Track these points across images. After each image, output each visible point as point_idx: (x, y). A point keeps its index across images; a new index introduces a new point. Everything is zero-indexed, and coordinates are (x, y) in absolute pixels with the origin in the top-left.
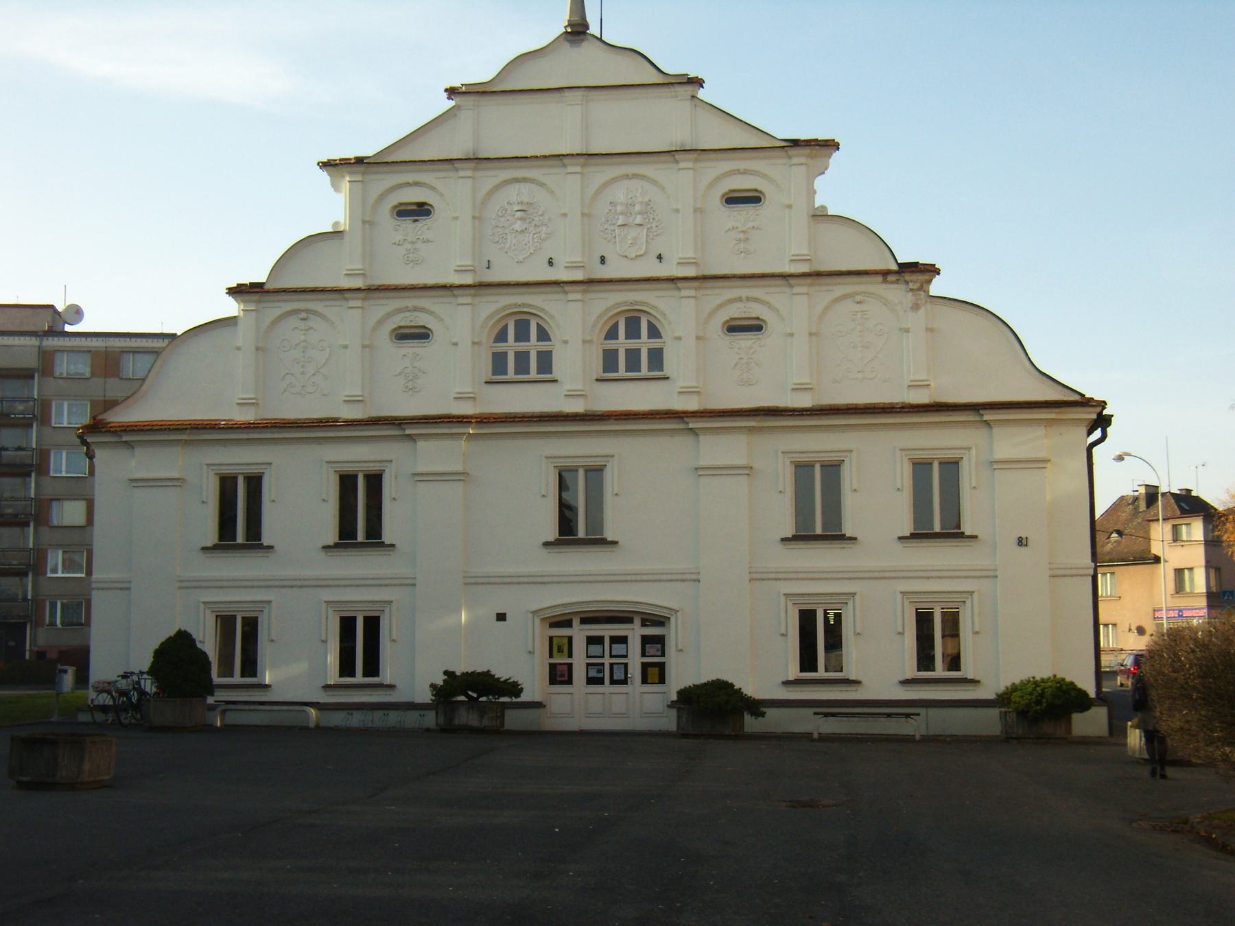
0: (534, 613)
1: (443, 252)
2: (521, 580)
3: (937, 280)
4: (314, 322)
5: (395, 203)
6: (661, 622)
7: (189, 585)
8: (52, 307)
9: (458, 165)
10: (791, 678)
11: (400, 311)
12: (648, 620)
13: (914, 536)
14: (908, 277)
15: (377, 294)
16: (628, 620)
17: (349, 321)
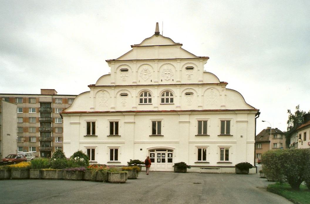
1: (129, 79)
5: (186, 67)
6: (171, 151)
11: (122, 90)
16: (166, 150)
17: (113, 92)
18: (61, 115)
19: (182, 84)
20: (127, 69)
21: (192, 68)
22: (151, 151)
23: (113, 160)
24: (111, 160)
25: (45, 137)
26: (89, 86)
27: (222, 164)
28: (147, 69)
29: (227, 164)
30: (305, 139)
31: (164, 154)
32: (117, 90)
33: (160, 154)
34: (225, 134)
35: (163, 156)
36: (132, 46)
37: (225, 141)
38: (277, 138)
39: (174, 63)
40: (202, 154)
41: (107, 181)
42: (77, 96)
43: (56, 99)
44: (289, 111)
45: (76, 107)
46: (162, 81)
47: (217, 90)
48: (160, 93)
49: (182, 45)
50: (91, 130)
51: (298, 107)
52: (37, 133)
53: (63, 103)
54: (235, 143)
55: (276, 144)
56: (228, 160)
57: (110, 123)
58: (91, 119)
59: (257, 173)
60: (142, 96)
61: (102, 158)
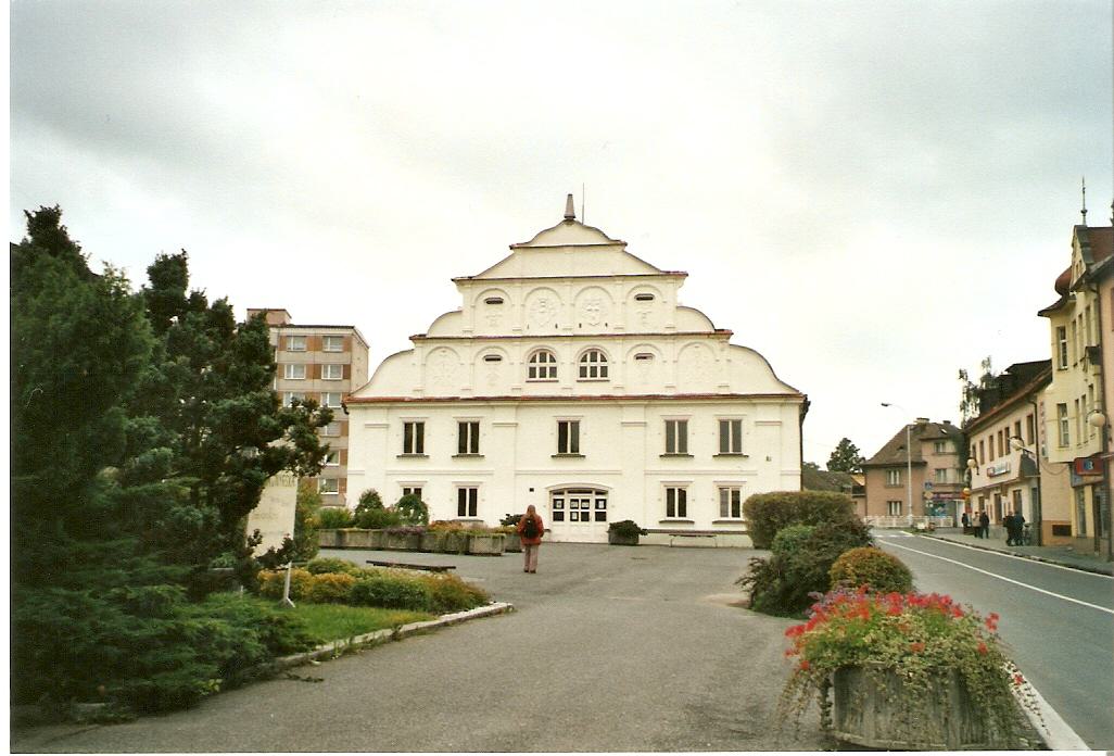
3: (732, 337)
7: (389, 474)
16: (591, 492)
17: (468, 353)
19: (626, 335)
26: (411, 338)
30: (983, 463)
31: (588, 501)
33: (577, 500)
35: (585, 505)
38: (944, 454)
39: (609, 286)
40: (677, 501)
41: (467, 553)
44: (962, 375)
47: (709, 347)
49: (626, 244)
50: (414, 441)
51: (986, 363)
54: (754, 474)
55: (945, 470)
58: (414, 415)
61: (441, 507)
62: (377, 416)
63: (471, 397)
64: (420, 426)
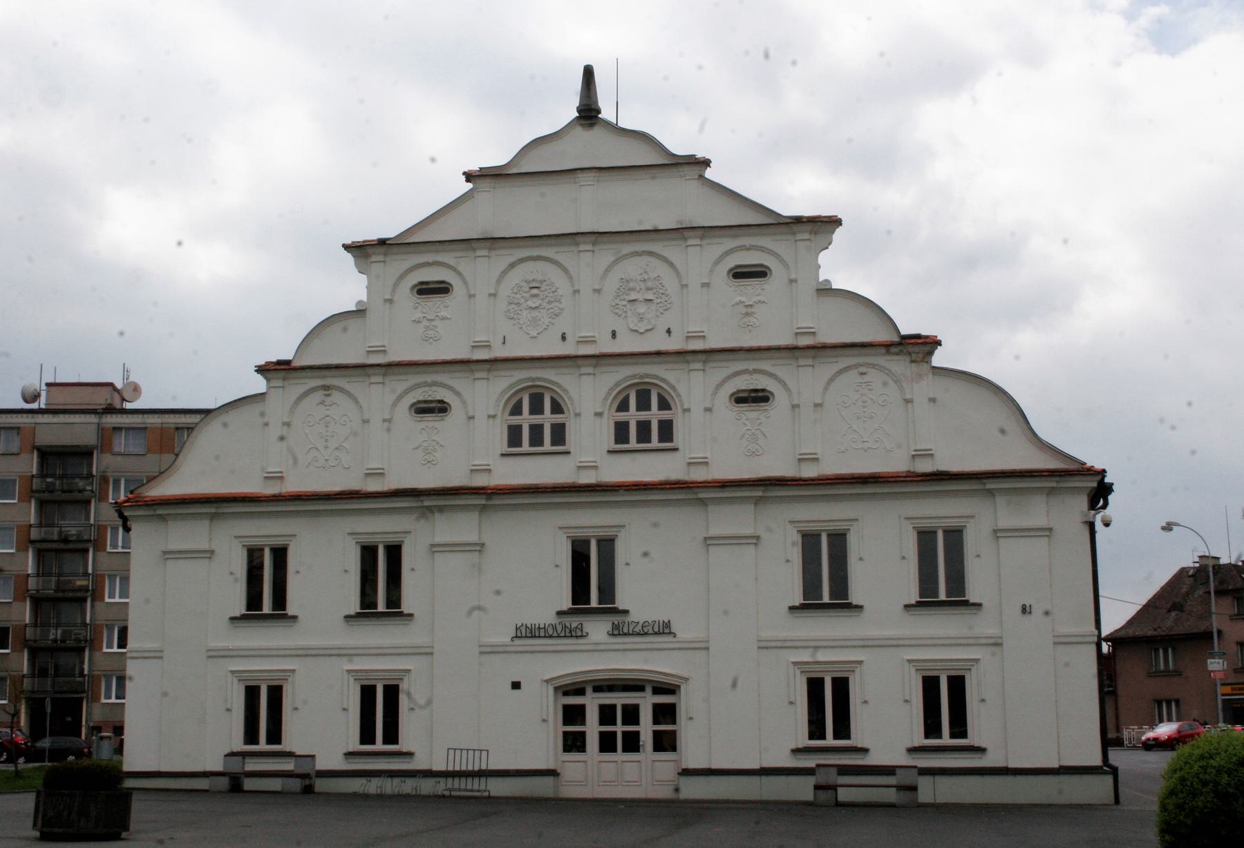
0: (547, 681)
1: (450, 331)
2: (901, 642)
3: (939, 352)
4: (336, 396)
5: (732, 265)
6: (671, 690)
7: (216, 655)
8: (111, 385)
9: (475, 244)
10: (800, 746)
11: (418, 386)
12: (659, 689)
13: (919, 604)
14: (910, 348)
15: (396, 370)
17: (379, 397)
18: (121, 515)
19: (390, 365)
20: (762, 265)
21: (759, 273)
22: (566, 694)
23: (940, 737)
24: (927, 737)
25: (57, 626)
27: (278, 760)
28: (541, 282)
29: (271, 760)
32: (399, 384)
34: (826, 599)
36: (469, 176)
37: (942, 639)
42: (211, 415)
43: (117, 429)
45: (192, 475)
46: (614, 334)
48: (609, 394)
49: (706, 163)
50: (266, 588)
52: (17, 605)
53: (149, 451)
56: (279, 742)
57: (916, 535)
59: (1117, 801)
60: (516, 410)
61: (322, 729)
62: (188, 534)
63: (385, 488)
64: (280, 554)
